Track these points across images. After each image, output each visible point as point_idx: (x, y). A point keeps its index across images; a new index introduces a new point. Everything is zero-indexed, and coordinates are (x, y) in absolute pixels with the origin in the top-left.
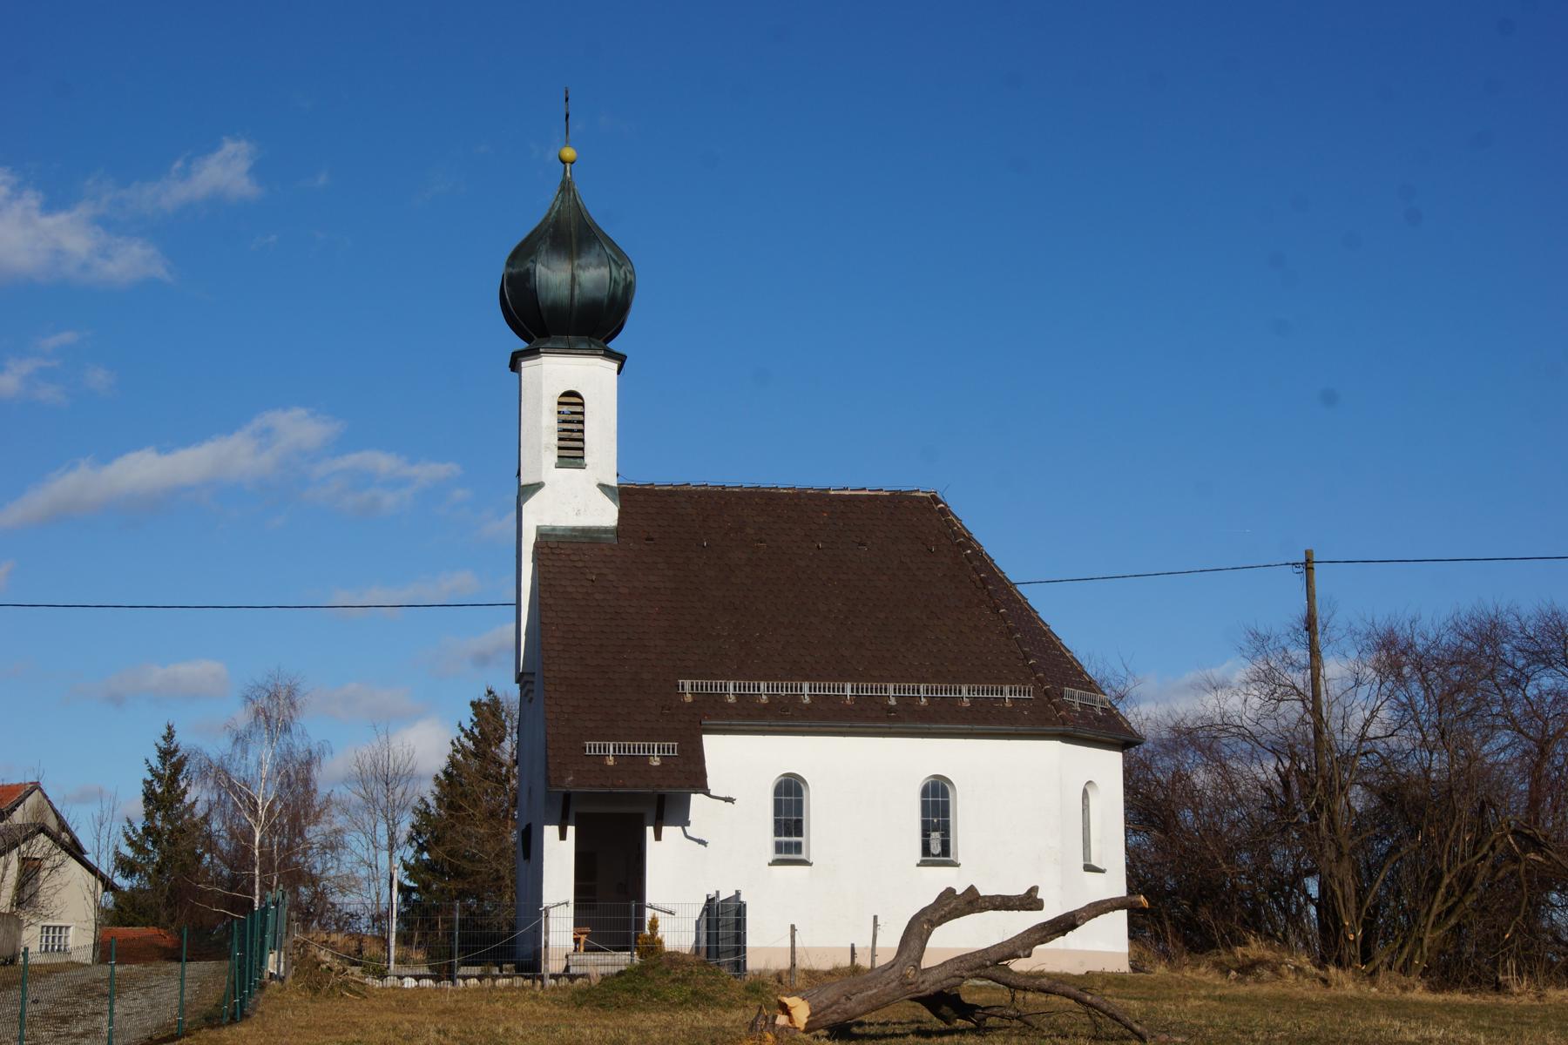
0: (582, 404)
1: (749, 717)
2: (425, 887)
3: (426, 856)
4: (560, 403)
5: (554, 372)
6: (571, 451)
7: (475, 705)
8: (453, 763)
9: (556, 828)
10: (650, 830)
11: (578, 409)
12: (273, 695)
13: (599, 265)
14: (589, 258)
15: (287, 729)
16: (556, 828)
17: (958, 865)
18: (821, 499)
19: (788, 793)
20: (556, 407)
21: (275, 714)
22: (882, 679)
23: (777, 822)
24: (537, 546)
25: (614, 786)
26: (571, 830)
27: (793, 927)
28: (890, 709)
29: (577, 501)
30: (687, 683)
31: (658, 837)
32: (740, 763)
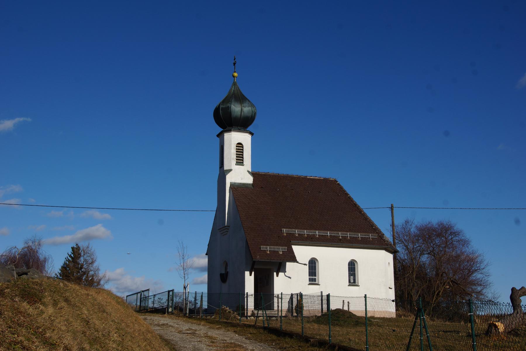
0: (243, 147)
1: (303, 240)
5: (234, 138)
6: (240, 161)
7: (73, 248)
8: (65, 263)
9: (248, 272)
10: (275, 274)
11: (241, 148)
13: (249, 107)
14: (246, 104)
16: (248, 272)
18: (305, 178)
20: (235, 148)
23: (309, 272)
24: (230, 187)
26: (253, 273)
28: (340, 240)
29: (240, 175)
30: (285, 230)
31: (277, 276)
32: (303, 253)
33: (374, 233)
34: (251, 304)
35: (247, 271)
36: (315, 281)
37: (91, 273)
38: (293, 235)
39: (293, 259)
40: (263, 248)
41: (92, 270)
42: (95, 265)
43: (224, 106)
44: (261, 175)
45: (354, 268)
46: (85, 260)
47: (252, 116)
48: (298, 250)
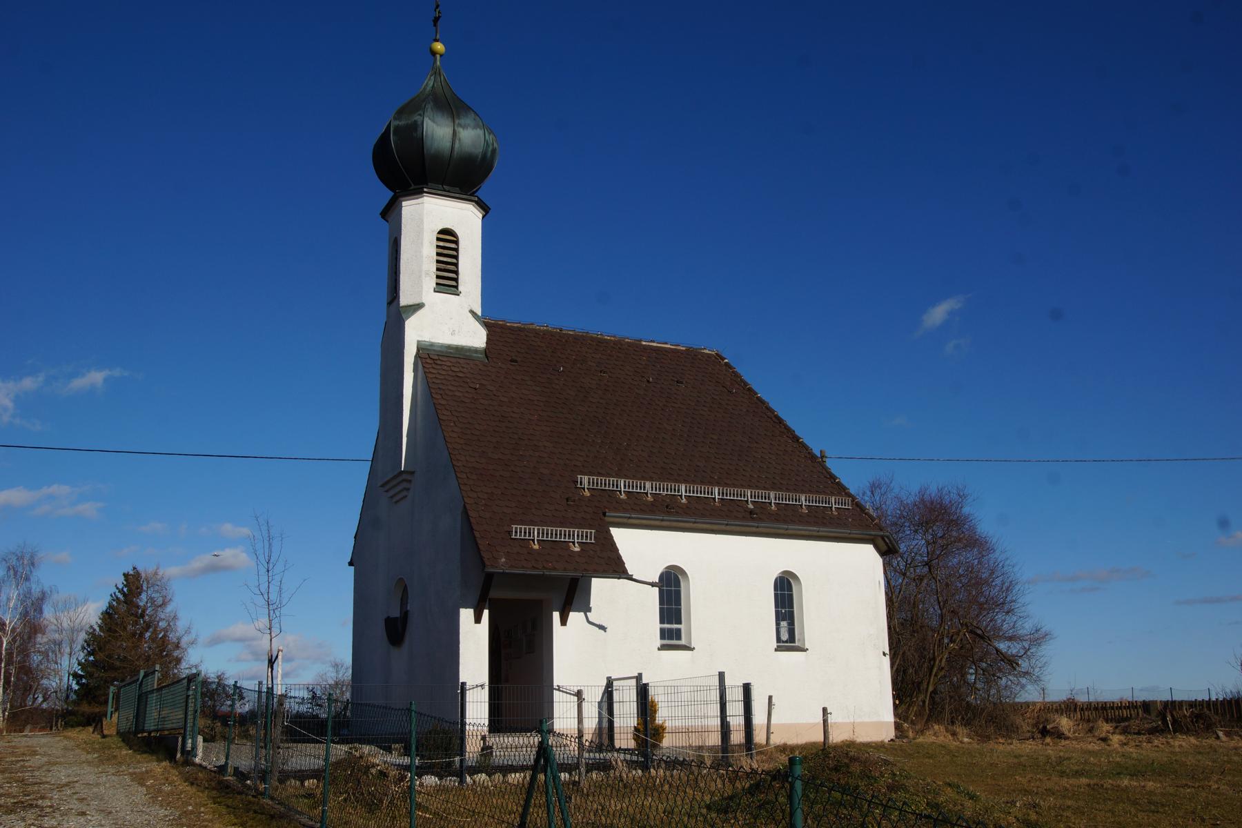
0: (456, 242)
1: (642, 511)
2: (89, 675)
3: (92, 658)
4: (438, 239)
5: (429, 215)
6: (448, 279)
7: (126, 575)
8: (111, 606)
10: (556, 616)
12: (20, 558)
13: (475, 127)
14: (468, 120)
15: (27, 579)
17: (806, 650)
18: (636, 348)
19: (669, 585)
20: (435, 243)
21: (20, 570)
22: (742, 486)
23: (661, 610)
24: (418, 356)
25: (544, 568)
26: (486, 613)
27: (825, 710)
28: (751, 512)
29: (447, 320)
30: (586, 479)
31: (564, 622)
32: (646, 549)
33: (839, 494)
34: (477, 710)
35: (466, 607)
36: (679, 638)
37: (162, 624)
38: (611, 495)
39: (615, 568)
40: (519, 532)
41: (161, 620)
42: (169, 609)
43: (402, 123)
44: (510, 328)
45: (791, 597)
46: (152, 600)
47: (484, 155)
48: (626, 540)
